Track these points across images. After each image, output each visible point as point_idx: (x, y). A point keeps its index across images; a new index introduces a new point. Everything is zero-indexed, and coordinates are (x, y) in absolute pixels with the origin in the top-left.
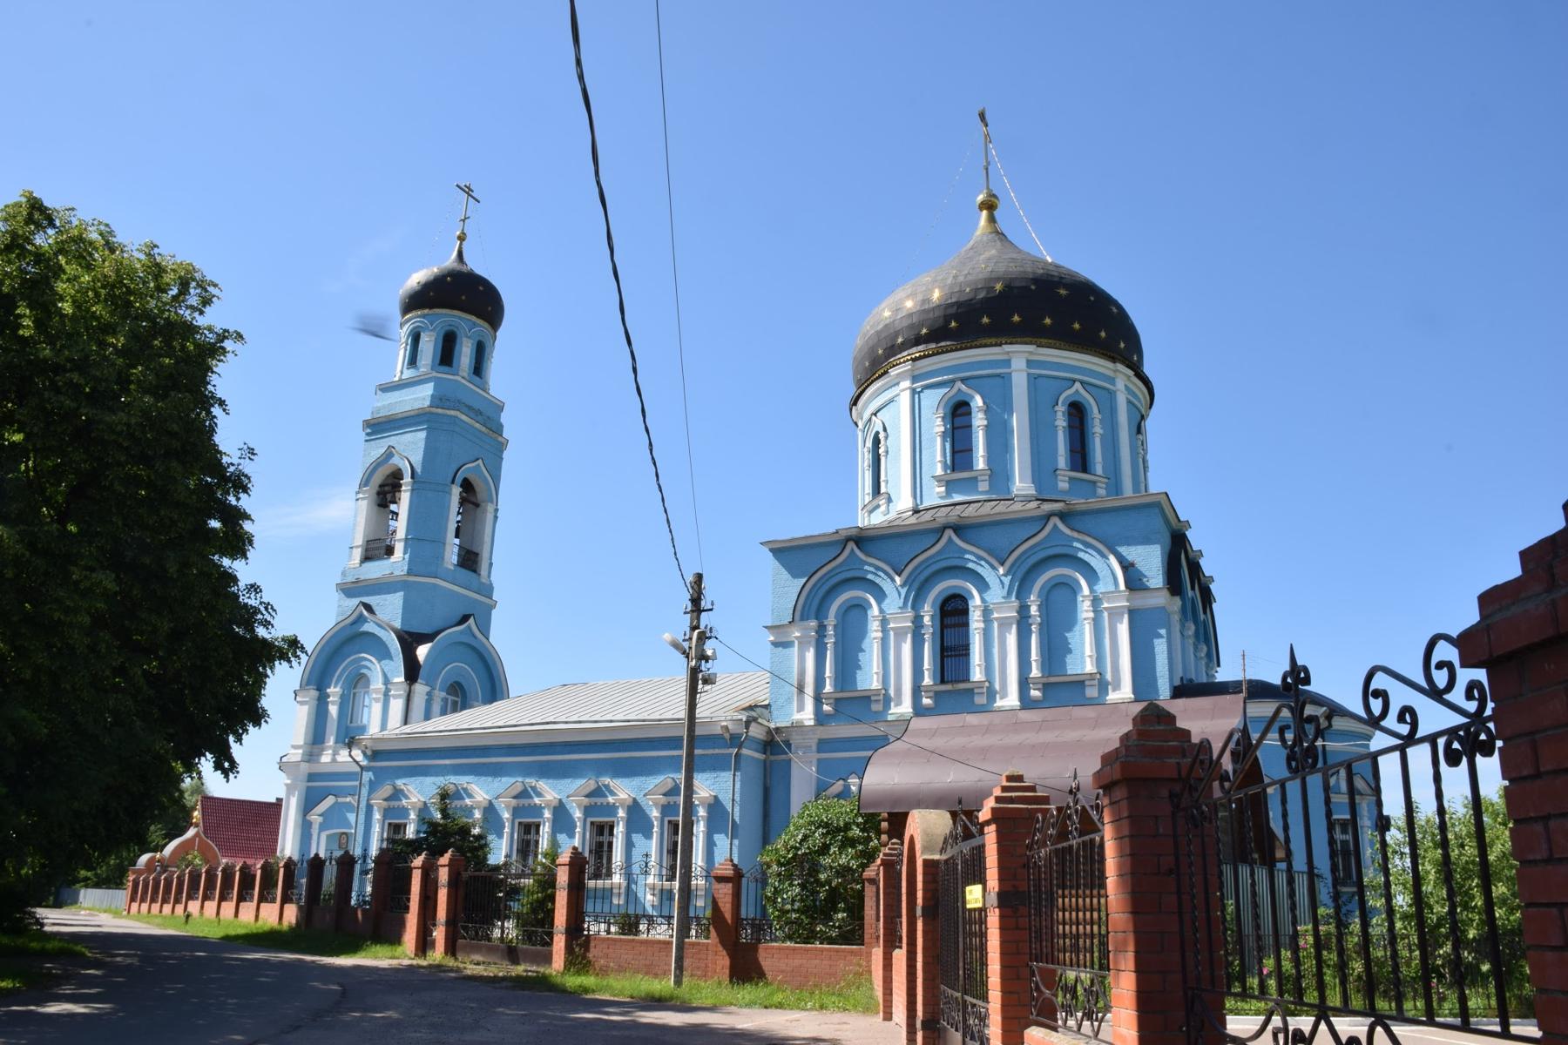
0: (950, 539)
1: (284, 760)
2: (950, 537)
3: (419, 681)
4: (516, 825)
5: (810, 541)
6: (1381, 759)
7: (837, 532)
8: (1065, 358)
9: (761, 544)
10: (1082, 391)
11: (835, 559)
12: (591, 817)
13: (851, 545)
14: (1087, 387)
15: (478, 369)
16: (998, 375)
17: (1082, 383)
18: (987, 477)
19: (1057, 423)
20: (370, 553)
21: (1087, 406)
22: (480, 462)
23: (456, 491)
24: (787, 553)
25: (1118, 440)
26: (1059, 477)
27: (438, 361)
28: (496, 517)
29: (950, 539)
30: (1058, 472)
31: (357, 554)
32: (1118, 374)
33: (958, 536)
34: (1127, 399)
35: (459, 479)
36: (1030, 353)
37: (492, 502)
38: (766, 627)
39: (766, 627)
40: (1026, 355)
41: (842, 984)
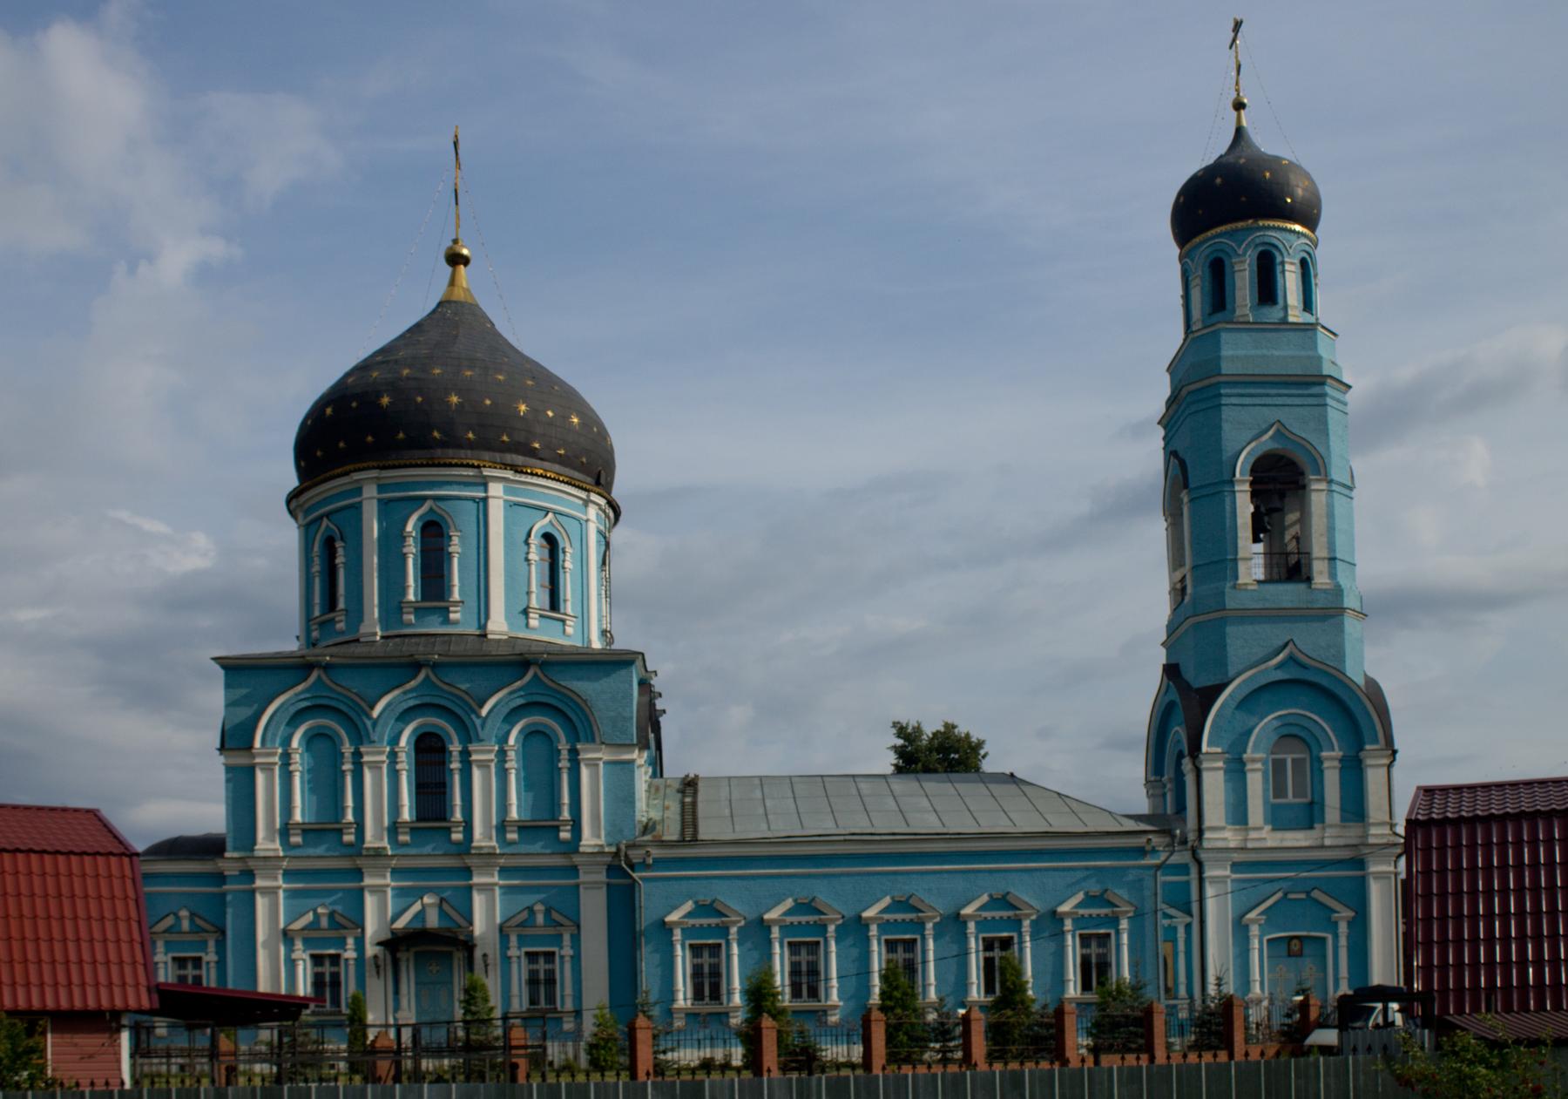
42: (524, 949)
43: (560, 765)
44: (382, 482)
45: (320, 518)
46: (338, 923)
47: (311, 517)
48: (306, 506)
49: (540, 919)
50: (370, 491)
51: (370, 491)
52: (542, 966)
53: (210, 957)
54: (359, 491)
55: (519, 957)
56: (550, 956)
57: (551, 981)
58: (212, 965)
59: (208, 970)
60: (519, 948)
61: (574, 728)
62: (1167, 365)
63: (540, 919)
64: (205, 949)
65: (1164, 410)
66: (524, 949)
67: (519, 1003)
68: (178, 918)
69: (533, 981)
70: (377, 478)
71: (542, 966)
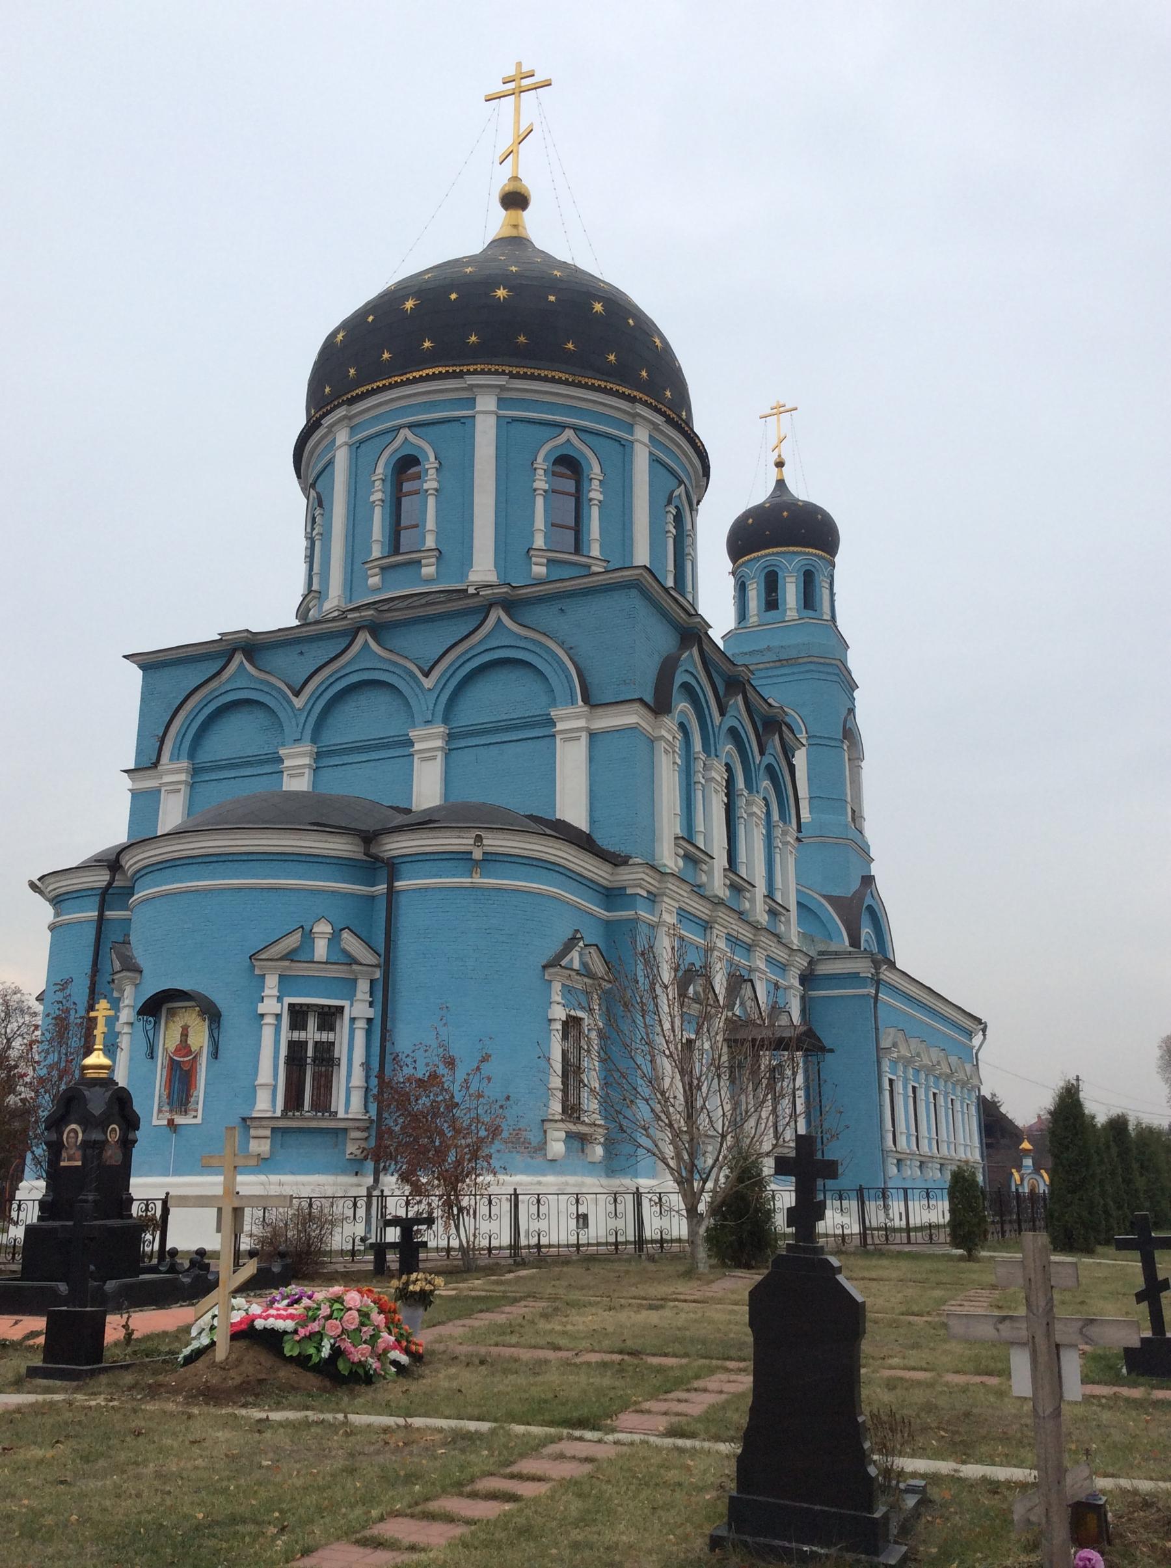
0: (366, 644)
2: (499, 618)
9: (124, 657)
10: (576, 441)
11: (467, 637)
12: (289, 996)
13: (239, 658)
14: (584, 436)
15: (809, 600)
17: (575, 429)
18: (433, 560)
19: (536, 485)
21: (583, 462)
25: (346, 546)
26: (534, 559)
30: (532, 552)
32: (638, 419)
33: (511, 617)
34: (651, 453)
38: (125, 771)
39: (125, 771)
40: (345, 422)
42: (288, 1000)
43: (373, 498)
44: (506, 395)
45: (398, 429)
46: (346, 953)
47: (359, 436)
48: (356, 421)
49: (321, 949)
50: (487, 403)
51: (487, 403)
52: (312, 1034)
53: (359, 1008)
54: (472, 402)
55: (278, 1016)
56: (329, 1017)
57: (326, 1056)
58: (361, 1024)
59: (352, 1031)
60: (280, 999)
61: (540, 673)
62: (295, 476)
63: (321, 949)
64: (351, 996)
65: (306, 501)
66: (288, 1000)
67: (743, 1097)
68: (308, 936)
69: (296, 1054)
70: (345, 417)
71: (312, 1034)
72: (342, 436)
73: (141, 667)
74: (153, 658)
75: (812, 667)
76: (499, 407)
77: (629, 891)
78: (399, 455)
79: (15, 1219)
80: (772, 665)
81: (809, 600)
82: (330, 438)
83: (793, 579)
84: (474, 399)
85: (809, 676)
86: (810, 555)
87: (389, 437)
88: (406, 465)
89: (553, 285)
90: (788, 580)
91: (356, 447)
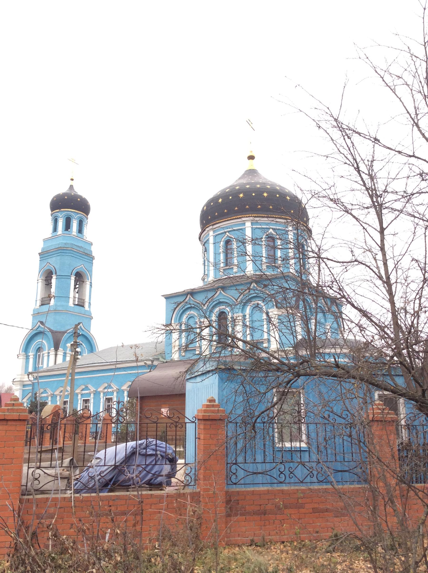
1: (14, 380)
3: (60, 349)
4: (82, 401)
5: (171, 295)
6: (187, 424)
7: (184, 291)
8: (48, 256)
15: (80, 231)
16: (241, 229)
20: (43, 303)
22: (82, 265)
23: (73, 278)
24: (168, 297)
27: (64, 229)
28: (91, 285)
29: (190, 298)
31: (39, 303)
35: (74, 272)
36: (252, 220)
37: (89, 280)
41: (405, 352)
50: (248, 224)
51: (248, 224)
72: (211, 233)
73: (165, 298)
74: (168, 296)
75: (72, 252)
76: (252, 225)
77: (297, 378)
78: (226, 239)
79: (167, 460)
80: (56, 249)
81: (80, 231)
82: (207, 234)
83: (62, 221)
84: (245, 223)
85: (70, 254)
86: (81, 214)
87: (223, 235)
88: (228, 242)
89: (279, 193)
90: (60, 221)
91: (215, 237)
